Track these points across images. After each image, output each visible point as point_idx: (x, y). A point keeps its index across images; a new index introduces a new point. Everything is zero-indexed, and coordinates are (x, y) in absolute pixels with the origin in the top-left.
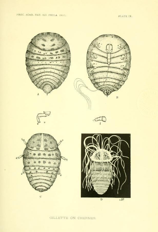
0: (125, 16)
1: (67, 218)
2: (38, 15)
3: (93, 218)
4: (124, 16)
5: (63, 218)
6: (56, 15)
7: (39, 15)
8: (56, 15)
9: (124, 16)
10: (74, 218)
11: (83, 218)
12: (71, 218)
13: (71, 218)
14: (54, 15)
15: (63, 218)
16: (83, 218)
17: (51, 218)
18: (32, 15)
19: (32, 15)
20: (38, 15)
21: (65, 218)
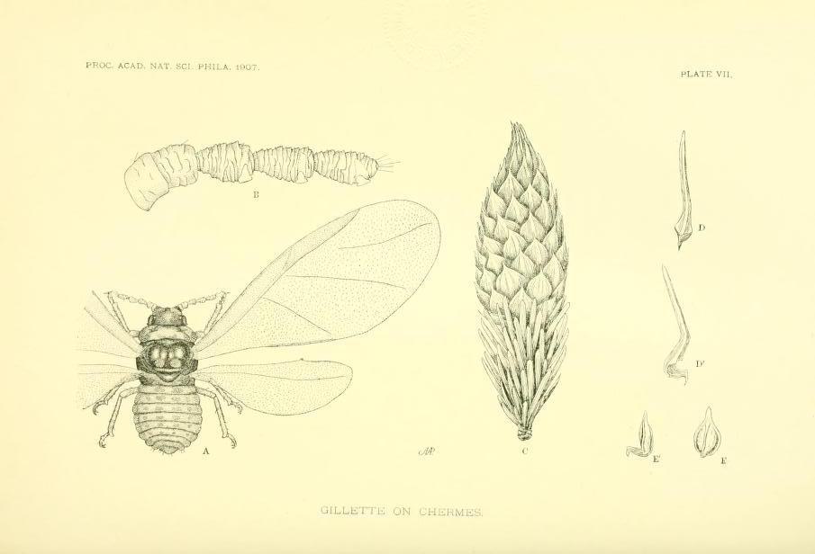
0: (705, 74)
1: (153, 66)
7: (164, 66)
12: (360, 168)
15: (367, 512)
18: (139, 66)
19: (139, 66)
21: (705, 74)
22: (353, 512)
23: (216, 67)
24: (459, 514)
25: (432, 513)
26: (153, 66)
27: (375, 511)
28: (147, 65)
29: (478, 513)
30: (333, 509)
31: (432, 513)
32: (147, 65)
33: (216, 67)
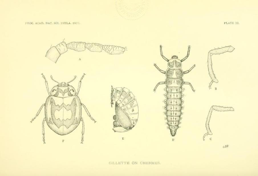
0: (232, 23)
1: (46, 23)
2: (229, 23)
3: (157, 163)
4: (230, 23)
5: (228, 23)
6: (69, 23)
7: (50, 23)
8: (69, 23)
9: (230, 23)
10: (55, 23)
11: (155, 163)
12: (51, 77)
13: (133, 163)
14: (65, 23)
15: (118, 163)
16: (155, 163)
17: (110, 163)
18: (42, 23)
19: (42, 23)
20: (49, 23)
21: (232, 23)
22: (119, 163)
23: (66, 23)
24: (153, 163)
25: (144, 163)
26: (46, 23)
27: (126, 163)
28: (235, 23)
29: (159, 163)
30: (113, 163)
31: (144, 163)
32: (34, 23)
33: (66, 23)
